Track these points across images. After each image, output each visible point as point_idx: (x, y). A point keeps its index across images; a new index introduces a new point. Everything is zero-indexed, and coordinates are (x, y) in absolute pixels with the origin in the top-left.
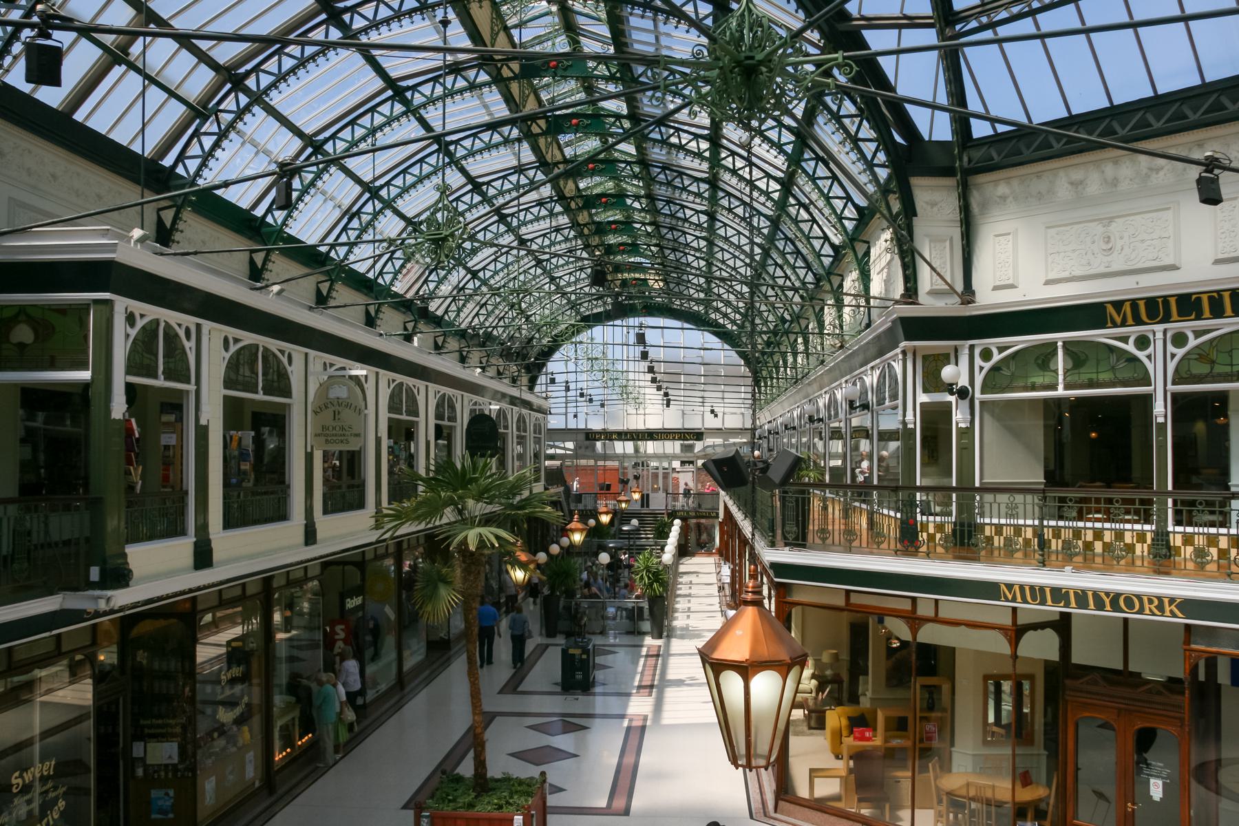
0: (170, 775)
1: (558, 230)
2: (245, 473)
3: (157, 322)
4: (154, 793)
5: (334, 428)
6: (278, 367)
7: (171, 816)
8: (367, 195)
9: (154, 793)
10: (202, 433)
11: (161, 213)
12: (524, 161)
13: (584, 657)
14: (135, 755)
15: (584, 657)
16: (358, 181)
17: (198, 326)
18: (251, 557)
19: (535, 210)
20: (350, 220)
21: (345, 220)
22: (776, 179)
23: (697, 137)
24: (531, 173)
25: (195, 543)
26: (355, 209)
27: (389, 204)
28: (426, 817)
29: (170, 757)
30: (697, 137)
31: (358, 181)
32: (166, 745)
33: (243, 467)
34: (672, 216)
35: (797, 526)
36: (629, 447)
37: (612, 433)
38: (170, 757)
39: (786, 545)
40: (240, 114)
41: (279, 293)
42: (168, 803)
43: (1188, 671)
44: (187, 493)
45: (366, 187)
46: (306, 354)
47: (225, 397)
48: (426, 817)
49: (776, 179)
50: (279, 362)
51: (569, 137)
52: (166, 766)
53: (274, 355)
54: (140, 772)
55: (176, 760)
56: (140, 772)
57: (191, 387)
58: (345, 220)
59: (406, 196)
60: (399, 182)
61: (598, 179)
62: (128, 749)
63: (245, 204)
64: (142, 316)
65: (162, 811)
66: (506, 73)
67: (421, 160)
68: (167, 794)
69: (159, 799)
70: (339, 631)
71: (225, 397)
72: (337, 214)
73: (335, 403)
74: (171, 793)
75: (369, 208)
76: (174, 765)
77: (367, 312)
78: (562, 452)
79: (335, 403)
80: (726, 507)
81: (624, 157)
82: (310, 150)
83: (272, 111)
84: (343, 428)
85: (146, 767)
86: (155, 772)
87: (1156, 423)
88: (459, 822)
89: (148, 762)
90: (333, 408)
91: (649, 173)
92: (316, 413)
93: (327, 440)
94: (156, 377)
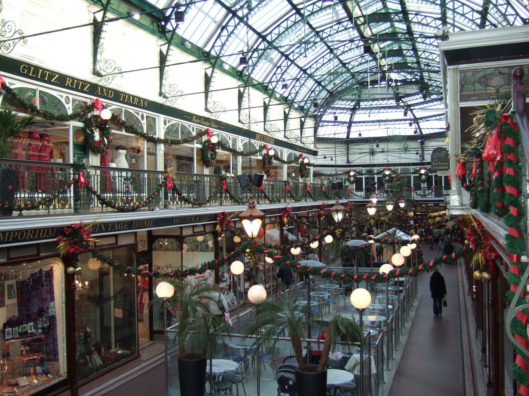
1: (352, 41)
8: (231, 15)
12: (340, 17)
19: (336, 27)
20: (253, 52)
22: (477, 12)
23: (435, 19)
24: (357, 42)
30: (435, 19)
34: (426, 58)
43: (504, 225)
49: (477, 12)
51: (374, 24)
60: (276, 31)
61: (389, 42)
66: (359, 22)
72: (214, 26)
75: (285, 64)
77: (285, 112)
80: (517, 305)
81: (401, 31)
82: (231, 15)
83: (355, 122)
87: (115, 318)
91: (417, 54)
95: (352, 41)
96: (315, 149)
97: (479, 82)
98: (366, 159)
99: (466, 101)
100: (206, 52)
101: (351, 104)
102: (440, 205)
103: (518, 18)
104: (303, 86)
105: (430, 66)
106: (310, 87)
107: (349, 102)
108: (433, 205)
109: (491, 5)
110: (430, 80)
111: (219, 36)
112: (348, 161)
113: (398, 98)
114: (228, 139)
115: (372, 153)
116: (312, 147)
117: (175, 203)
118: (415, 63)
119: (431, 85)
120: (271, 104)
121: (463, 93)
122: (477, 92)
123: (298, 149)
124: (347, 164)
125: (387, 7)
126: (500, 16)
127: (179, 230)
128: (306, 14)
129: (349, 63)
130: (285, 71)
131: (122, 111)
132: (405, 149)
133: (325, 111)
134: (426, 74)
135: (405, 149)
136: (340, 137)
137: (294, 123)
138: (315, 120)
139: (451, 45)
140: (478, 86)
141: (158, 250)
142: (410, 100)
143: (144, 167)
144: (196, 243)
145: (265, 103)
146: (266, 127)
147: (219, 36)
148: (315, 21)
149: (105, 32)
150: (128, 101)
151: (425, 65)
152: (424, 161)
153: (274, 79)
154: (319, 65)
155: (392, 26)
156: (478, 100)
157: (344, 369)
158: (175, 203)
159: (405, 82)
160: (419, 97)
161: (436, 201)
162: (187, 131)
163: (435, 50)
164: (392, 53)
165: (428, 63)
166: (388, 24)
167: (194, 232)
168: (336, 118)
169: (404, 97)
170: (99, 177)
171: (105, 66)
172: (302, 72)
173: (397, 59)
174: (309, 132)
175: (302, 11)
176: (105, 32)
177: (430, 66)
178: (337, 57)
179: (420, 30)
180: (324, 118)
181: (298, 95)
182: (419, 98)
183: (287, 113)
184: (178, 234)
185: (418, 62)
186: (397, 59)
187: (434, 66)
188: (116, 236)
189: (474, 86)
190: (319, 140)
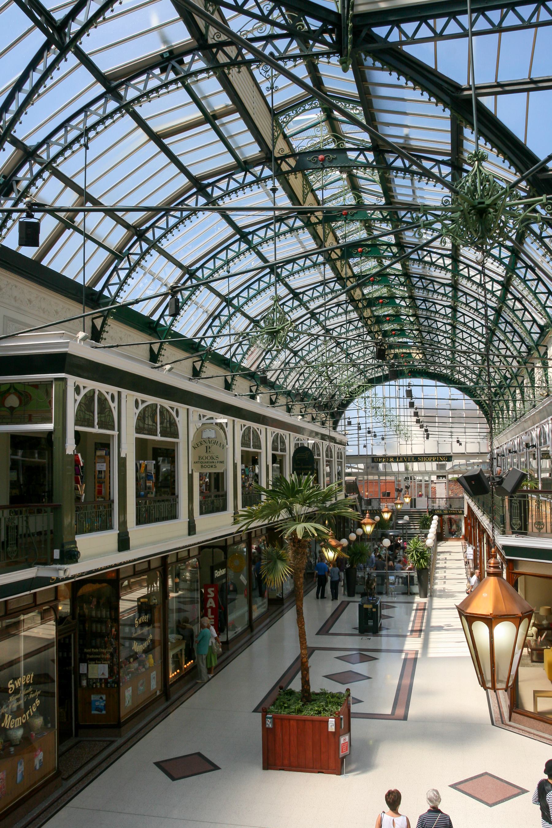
0: (103, 685)
2: (149, 488)
3: (93, 391)
4: (93, 697)
5: (207, 458)
6: (170, 418)
7: (104, 712)
9: (93, 697)
10: (122, 462)
11: (95, 321)
13: (374, 610)
14: (81, 672)
15: (374, 610)
16: (218, 294)
17: (119, 393)
18: (154, 543)
20: (214, 320)
21: (210, 321)
22: (498, 282)
25: (119, 534)
26: (287, 361)
27: (238, 309)
28: (270, 718)
29: (103, 674)
30: (442, 256)
31: (218, 294)
32: (100, 666)
33: (148, 484)
35: (521, 520)
36: (401, 467)
37: (389, 457)
38: (103, 674)
39: (513, 533)
40: (143, 256)
41: (170, 370)
42: (103, 704)
44: (113, 501)
45: (224, 298)
46: (188, 409)
47: (137, 439)
48: (270, 718)
49: (498, 282)
50: (170, 415)
52: (101, 679)
53: (167, 410)
54: (84, 683)
55: (107, 676)
56: (84, 683)
57: (115, 433)
58: (210, 321)
59: (250, 303)
62: (77, 668)
63: (146, 313)
64: (84, 387)
65: (97, 709)
67: (227, 248)
68: (101, 698)
69: (98, 701)
70: (211, 593)
71: (137, 439)
72: (205, 316)
73: (207, 441)
74: (104, 697)
76: (106, 680)
78: (356, 471)
79: (207, 441)
84: (212, 458)
85: (88, 680)
86: (94, 683)
88: (292, 722)
89: (89, 677)
90: (206, 445)
91: (411, 281)
92: (194, 448)
93: (202, 466)
94: (93, 426)
95: (324, 283)
103: (535, 325)
104: (189, 302)
106: (211, 310)
109: (514, 237)
111: (210, 326)
115: (196, 374)
128: (129, 98)
130: (138, 263)
147: (264, 359)
149: (107, 332)
153: (209, 333)
154: (252, 293)
163: (442, 300)
172: (292, 355)
175: (250, 237)
176: (107, 332)
179: (420, 272)
181: (125, 287)
183: (156, 352)
184: (223, 544)
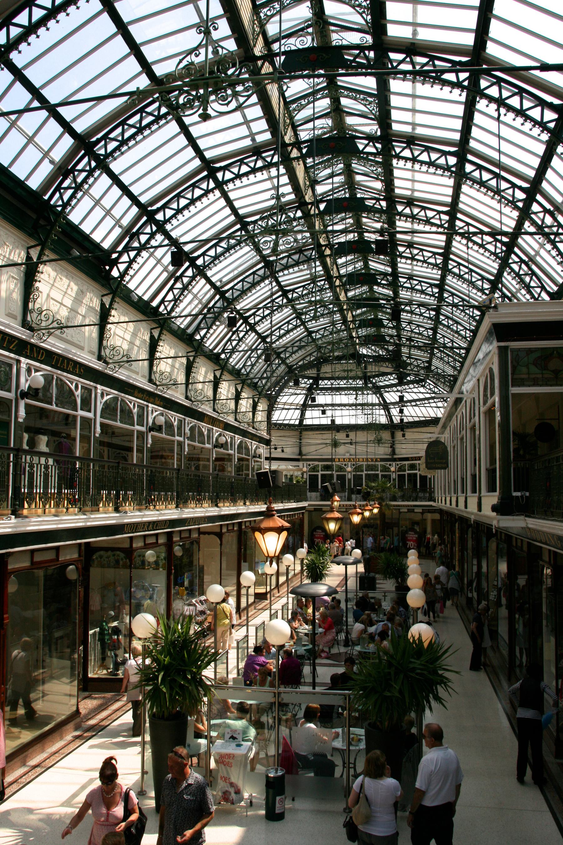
23: (431, 285)
30: (431, 285)
96: (267, 437)
97: (535, 364)
98: (327, 451)
99: (519, 386)
100: (153, 308)
101: (308, 382)
102: (416, 511)
105: (413, 341)
107: (306, 380)
108: (406, 510)
110: (409, 358)
111: (171, 289)
112: (300, 454)
113: (366, 378)
114: (173, 420)
116: (264, 434)
117: (33, 506)
118: (396, 336)
119: (411, 364)
120: (223, 377)
121: (515, 376)
122: (532, 376)
123: (250, 437)
124: (299, 457)
125: (369, 268)
126: (523, 288)
127: (129, 540)
129: (317, 332)
131: (53, 378)
132: (379, 440)
133: (281, 390)
134: (405, 350)
135: (379, 440)
136: (314, 423)
137: (245, 405)
138: (269, 400)
139: (500, 317)
140: (533, 369)
141: (138, 568)
142: (382, 382)
143: (75, 453)
144: (116, 558)
145: (215, 376)
146: (216, 407)
148: (286, 278)
150: (61, 364)
151: (407, 340)
152: (395, 457)
155: (371, 290)
156: (534, 385)
157: (5, 740)
158: (33, 506)
159: (378, 359)
160: (392, 378)
161: (411, 506)
162: (128, 408)
164: (364, 324)
165: (411, 337)
166: (365, 288)
167: (145, 544)
168: (401, 398)
169: (374, 377)
170: (43, 466)
171: (39, 318)
173: (371, 331)
174: (260, 416)
177: (413, 341)
178: (303, 323)
180: (282, 399)
182: (392, 379)
184: (127, 545)
185: (399, 336)
186: (371, 331)
187: (417, 341)
188: (57, 548)
189: (528, 368)
190: (271, 426)
